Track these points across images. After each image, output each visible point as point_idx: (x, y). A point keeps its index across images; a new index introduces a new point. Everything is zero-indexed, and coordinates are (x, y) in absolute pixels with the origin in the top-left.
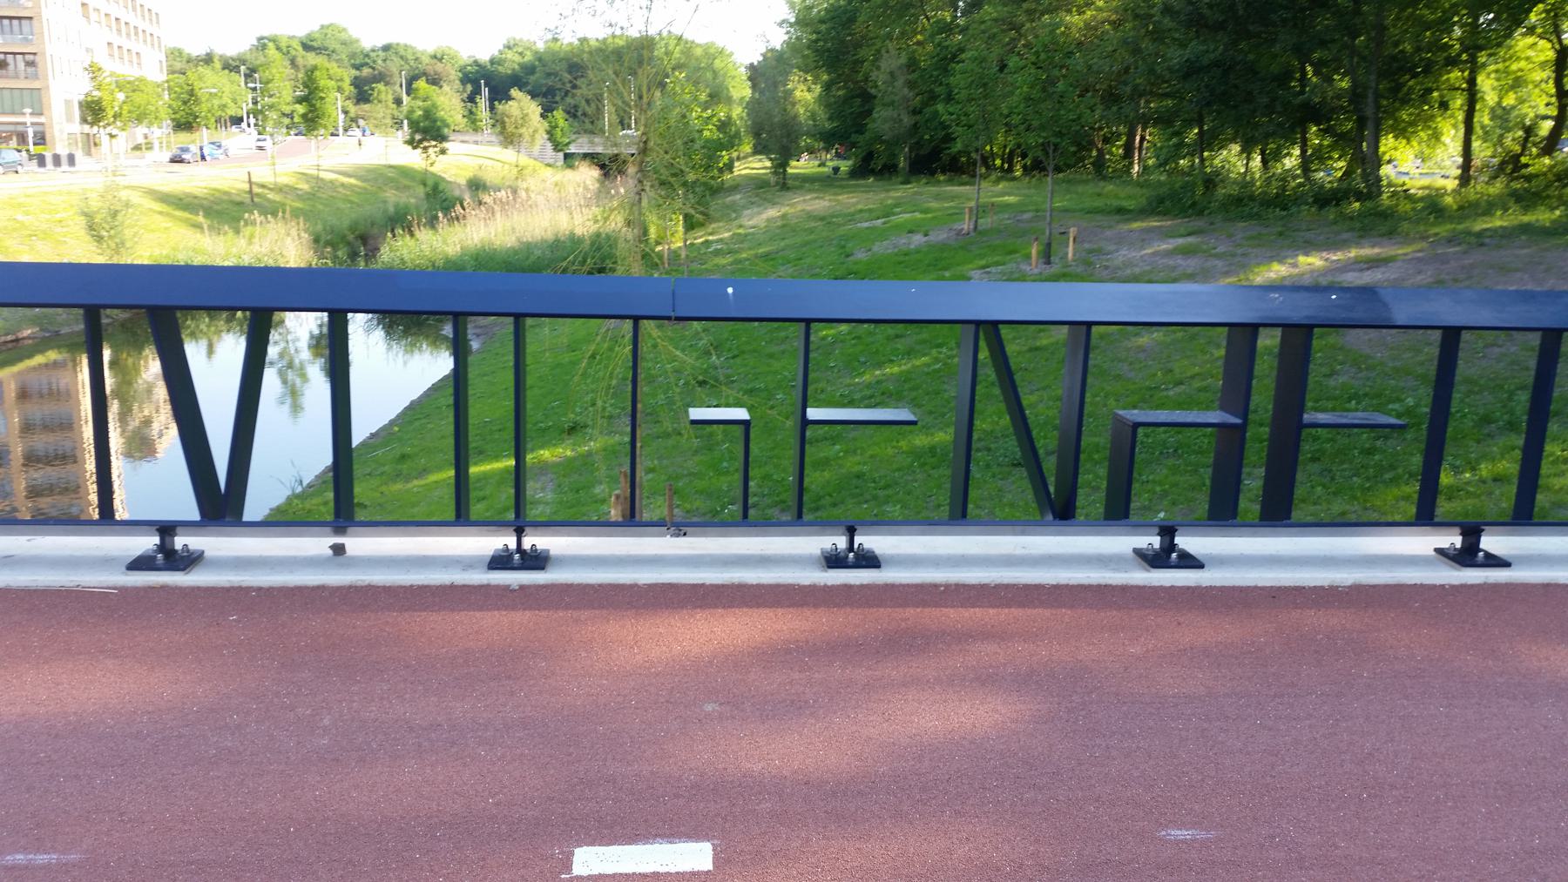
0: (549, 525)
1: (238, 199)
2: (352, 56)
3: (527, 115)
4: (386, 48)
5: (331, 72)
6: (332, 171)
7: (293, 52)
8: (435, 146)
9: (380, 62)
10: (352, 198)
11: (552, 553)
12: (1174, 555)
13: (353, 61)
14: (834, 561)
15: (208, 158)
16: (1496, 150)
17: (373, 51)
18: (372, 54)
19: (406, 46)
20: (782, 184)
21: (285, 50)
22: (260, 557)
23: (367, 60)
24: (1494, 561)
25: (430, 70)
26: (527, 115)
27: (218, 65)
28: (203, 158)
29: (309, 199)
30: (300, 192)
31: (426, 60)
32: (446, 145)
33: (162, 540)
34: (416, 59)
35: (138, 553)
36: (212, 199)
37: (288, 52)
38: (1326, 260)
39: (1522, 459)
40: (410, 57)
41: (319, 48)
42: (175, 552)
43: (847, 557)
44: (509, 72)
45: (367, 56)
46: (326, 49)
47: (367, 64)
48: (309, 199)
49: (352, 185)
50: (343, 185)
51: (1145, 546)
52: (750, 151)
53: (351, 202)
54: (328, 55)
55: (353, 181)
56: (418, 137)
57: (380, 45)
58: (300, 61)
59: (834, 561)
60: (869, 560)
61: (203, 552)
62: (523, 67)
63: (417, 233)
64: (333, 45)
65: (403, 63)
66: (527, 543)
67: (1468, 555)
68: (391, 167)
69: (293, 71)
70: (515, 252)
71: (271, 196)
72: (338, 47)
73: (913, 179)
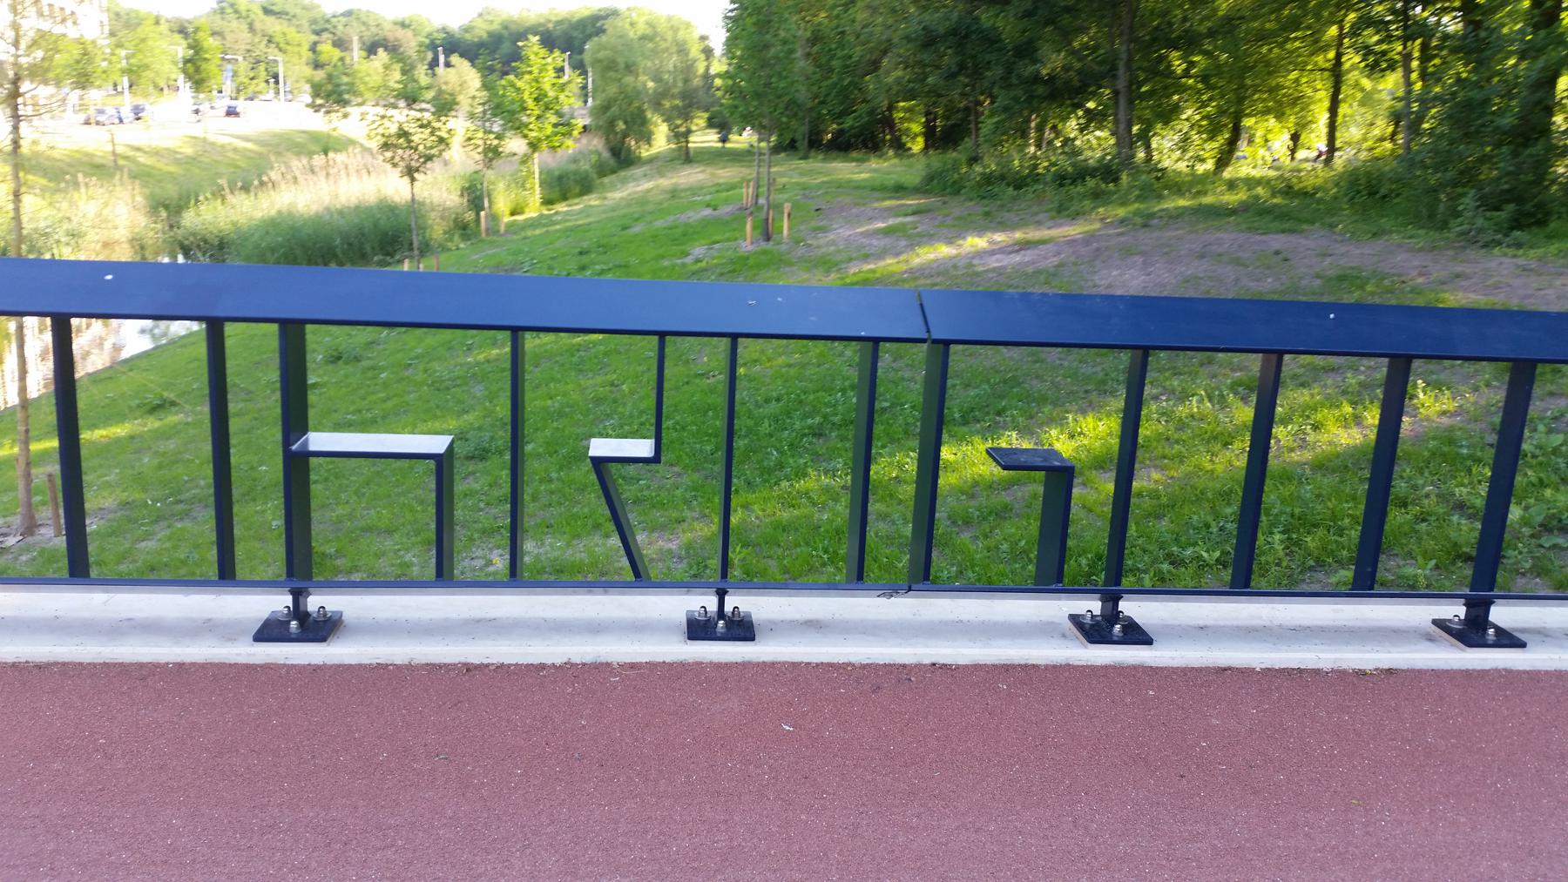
0: (757, 582)
1: (100, 161)
2: (314, 22)
3: (465, 82)
4: (349, 14)
5: (289, 37)
6: (238, 137)
7: (252, 16)
8: (337, 111)
9: (340, 27)
10: (239, 163)
11: (754, 618)
12: (1117, 627)
13: (313, 27)
14: (698, 629)
15: (125, 121)
16: (922, 79)
17: (334, 16)
18: (334, 20)
19: (368, 12)
20: (686, 157)
21: (244, 14)
22: (446, 620)
23: (328, 26)
24: (1507, 639)
25: (390, 36)
26: (465, 82)
27: (164, 28)
28: (121, 121)
29: (186, 163)
30: (179, 156)
31: (387, 26)
32: (348, 109)
33: (296, 602)
34: (378, 25)
35: (265, 615)
36: (68, 160)
37: (248, 17)
38: (605, 198)
39: (229, 449)
40: (372, 23)
41: (279, 13)
42: (307, 614)
43: (716, 624)
44: (476, 40)
45: (328, 21)
46: (287, 14)
47: (326, 30)
48: (186, 163)
49: (246, 150)
50: (235, 150)
51: (1451, 617)
52: (704, 125)
53: (237, 167)
54: (289, 20)
55: (250, 146)
56: (319, 101)
57: (341, 11)
58: (258, 26)
59: (698, 629)
60: (741, 629)
61: (341, 613)
62: (490, 34)
63: (229, 197)
64: (292, 10)
65: (364, 29)
66: (731, 602)
67: (1474, 631)
68: (304, 132)
69: (249, 35)
70: (318, 216)
71: (142, 159)
72: (298, 11)
73: (813, 153)
